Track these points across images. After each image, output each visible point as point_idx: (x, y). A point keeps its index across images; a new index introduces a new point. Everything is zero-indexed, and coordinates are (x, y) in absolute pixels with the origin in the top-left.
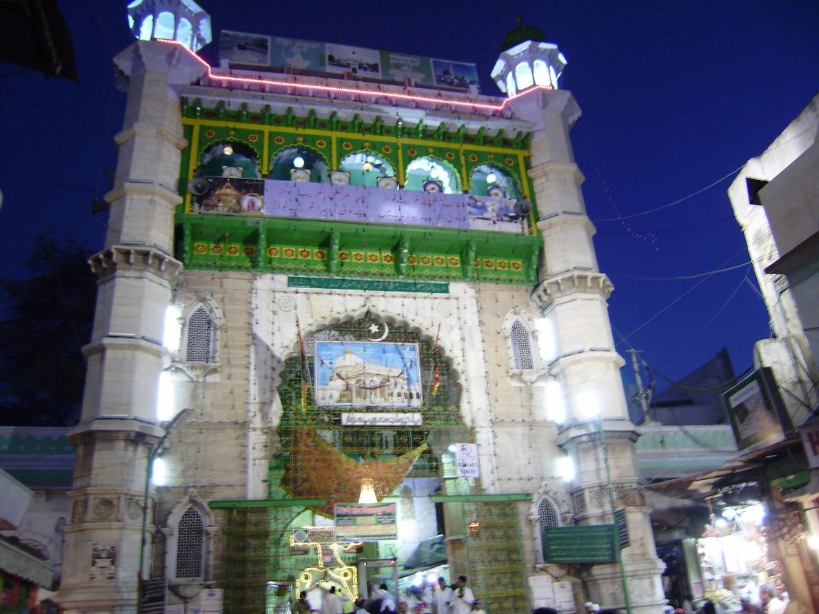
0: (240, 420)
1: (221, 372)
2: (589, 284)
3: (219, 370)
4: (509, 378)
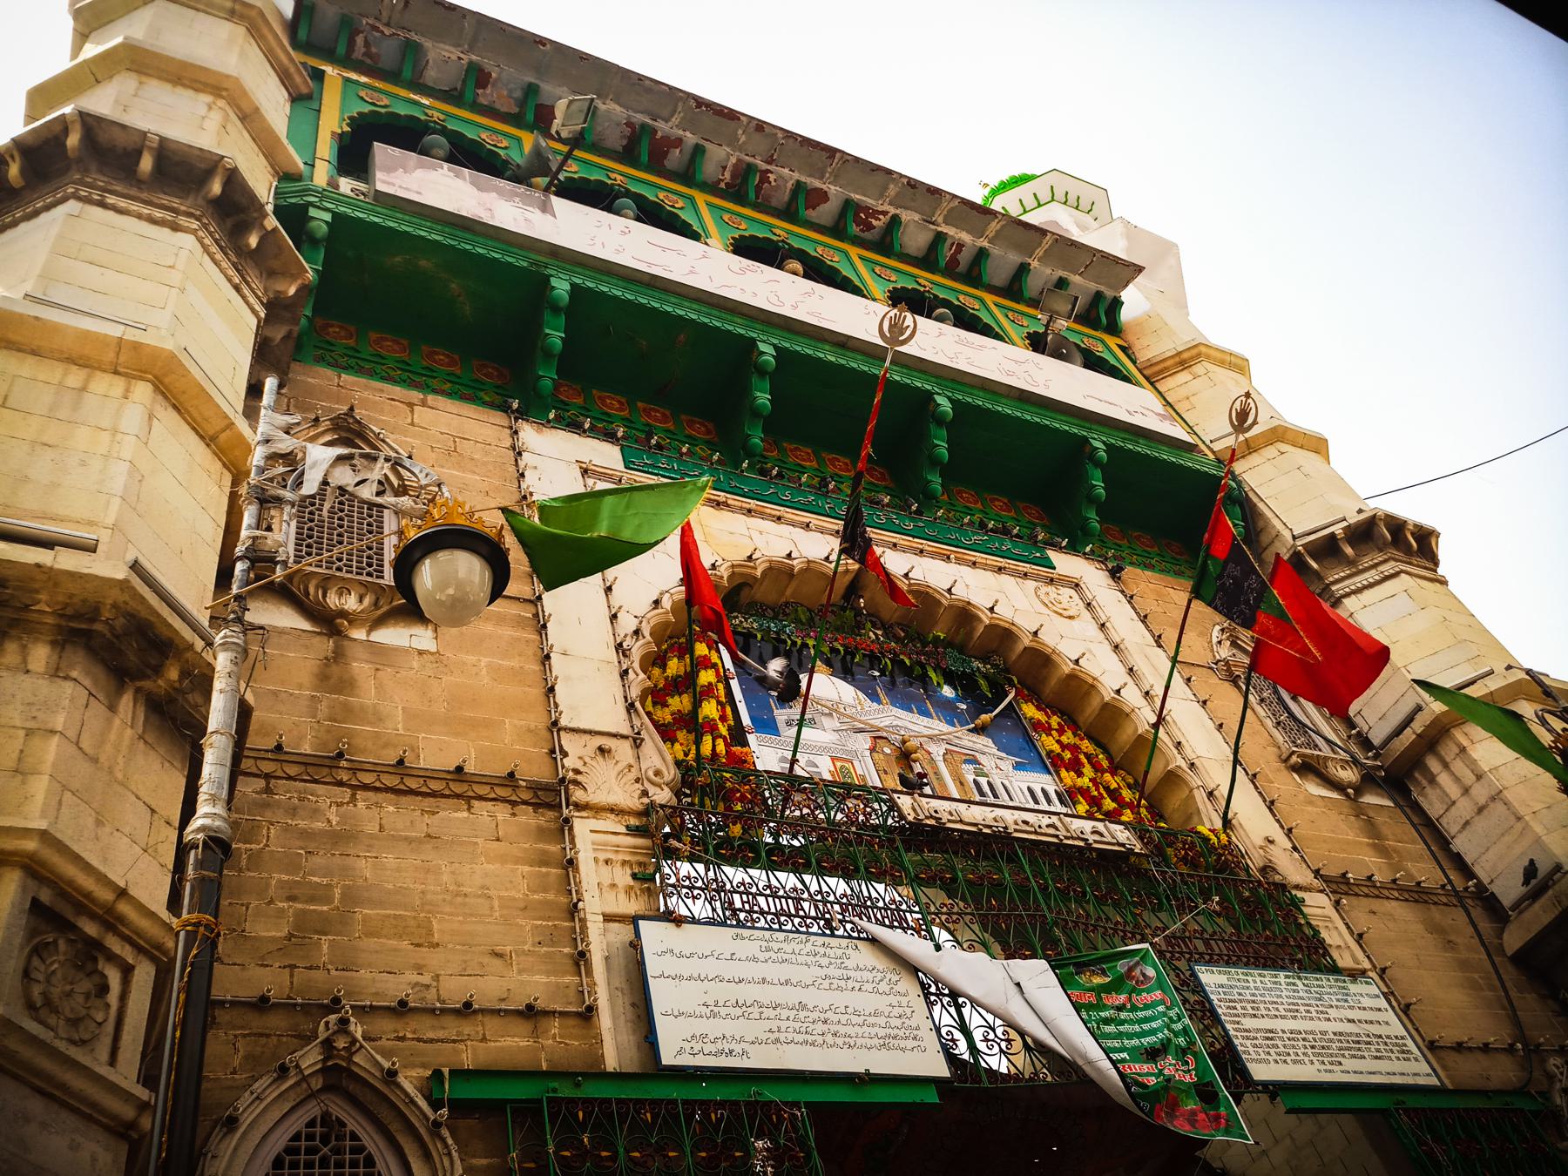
0: (535, 769)
2: (1349, 550)
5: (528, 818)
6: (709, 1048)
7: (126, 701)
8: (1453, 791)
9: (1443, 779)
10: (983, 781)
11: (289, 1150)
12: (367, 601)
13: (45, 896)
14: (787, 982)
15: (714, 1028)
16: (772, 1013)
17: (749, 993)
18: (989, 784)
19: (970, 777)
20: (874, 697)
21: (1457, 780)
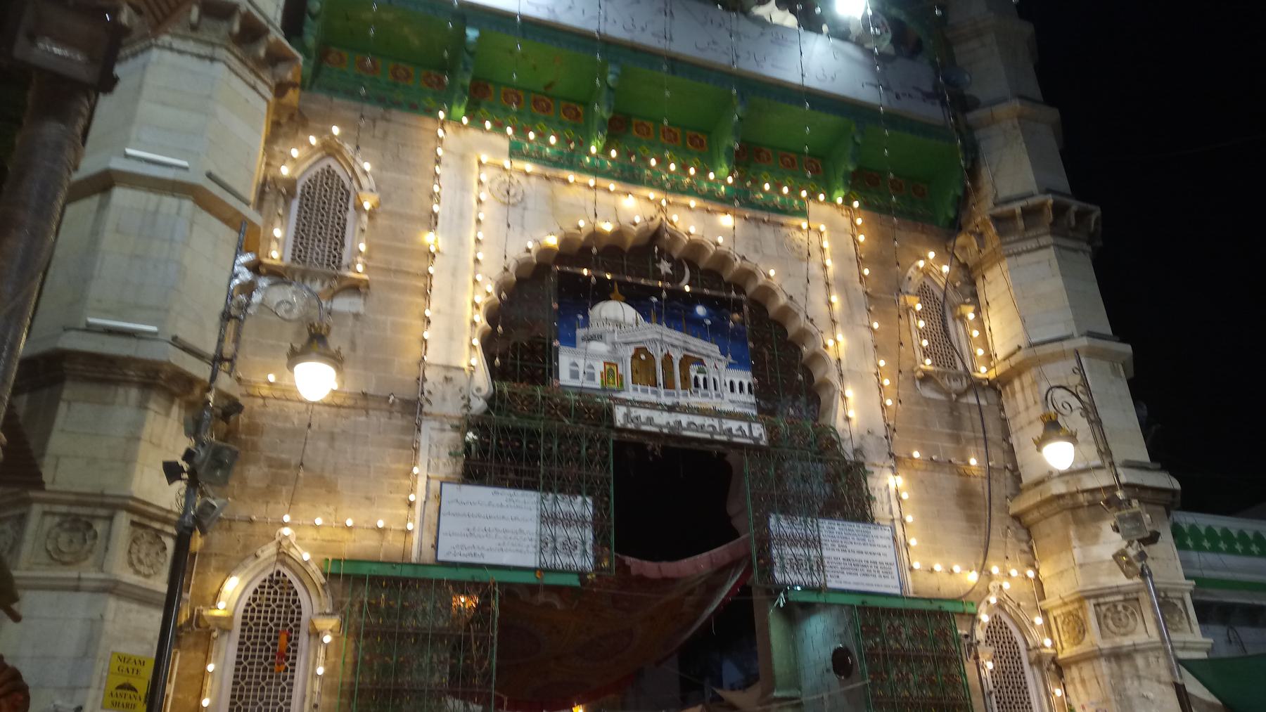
0: (409, 394)
1: (366, 294)
3: (362, 290)
4: (918, 383)
5: (398, 421)
6: (465, 552)
7: (175, 410)
8: (1022, 407)
9: (1019, 396)
10: (701, 377)
11: (261, 587)
12: (326, 285)
13: (136, 518)
14: (516, 518)
15: (469, 542)
16: (501, 535)
17: (491, 524)
18: (705, 379)
19: (693, 374)
20: (647, 317)
21: (1025, 400)
